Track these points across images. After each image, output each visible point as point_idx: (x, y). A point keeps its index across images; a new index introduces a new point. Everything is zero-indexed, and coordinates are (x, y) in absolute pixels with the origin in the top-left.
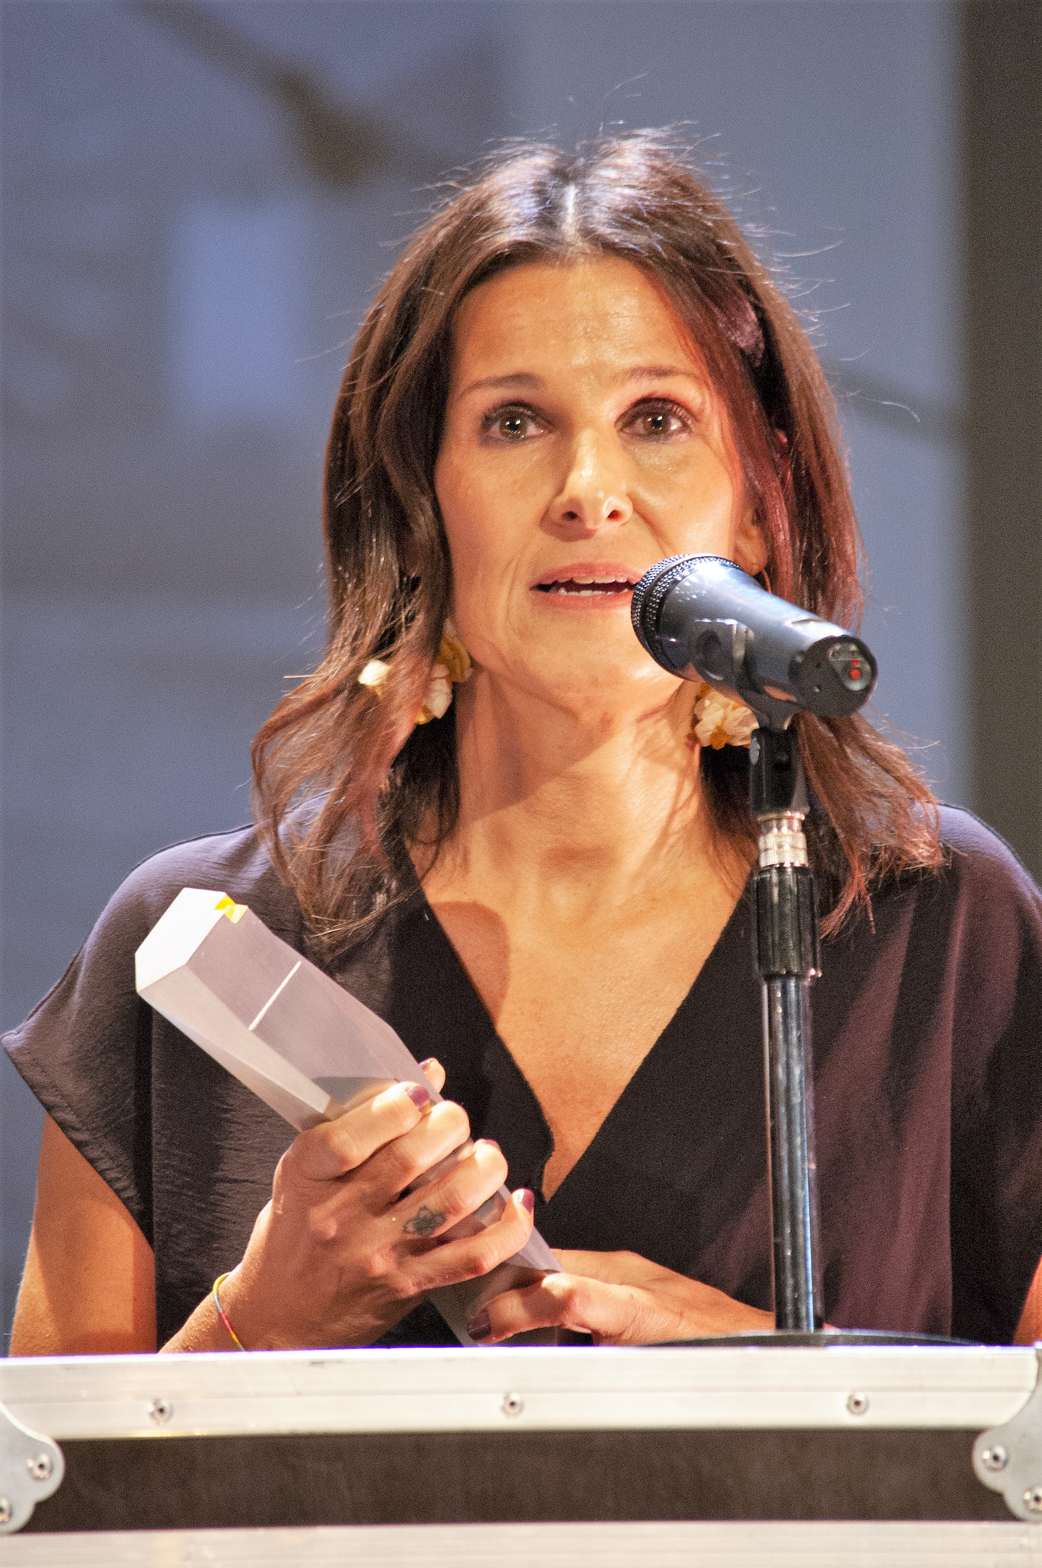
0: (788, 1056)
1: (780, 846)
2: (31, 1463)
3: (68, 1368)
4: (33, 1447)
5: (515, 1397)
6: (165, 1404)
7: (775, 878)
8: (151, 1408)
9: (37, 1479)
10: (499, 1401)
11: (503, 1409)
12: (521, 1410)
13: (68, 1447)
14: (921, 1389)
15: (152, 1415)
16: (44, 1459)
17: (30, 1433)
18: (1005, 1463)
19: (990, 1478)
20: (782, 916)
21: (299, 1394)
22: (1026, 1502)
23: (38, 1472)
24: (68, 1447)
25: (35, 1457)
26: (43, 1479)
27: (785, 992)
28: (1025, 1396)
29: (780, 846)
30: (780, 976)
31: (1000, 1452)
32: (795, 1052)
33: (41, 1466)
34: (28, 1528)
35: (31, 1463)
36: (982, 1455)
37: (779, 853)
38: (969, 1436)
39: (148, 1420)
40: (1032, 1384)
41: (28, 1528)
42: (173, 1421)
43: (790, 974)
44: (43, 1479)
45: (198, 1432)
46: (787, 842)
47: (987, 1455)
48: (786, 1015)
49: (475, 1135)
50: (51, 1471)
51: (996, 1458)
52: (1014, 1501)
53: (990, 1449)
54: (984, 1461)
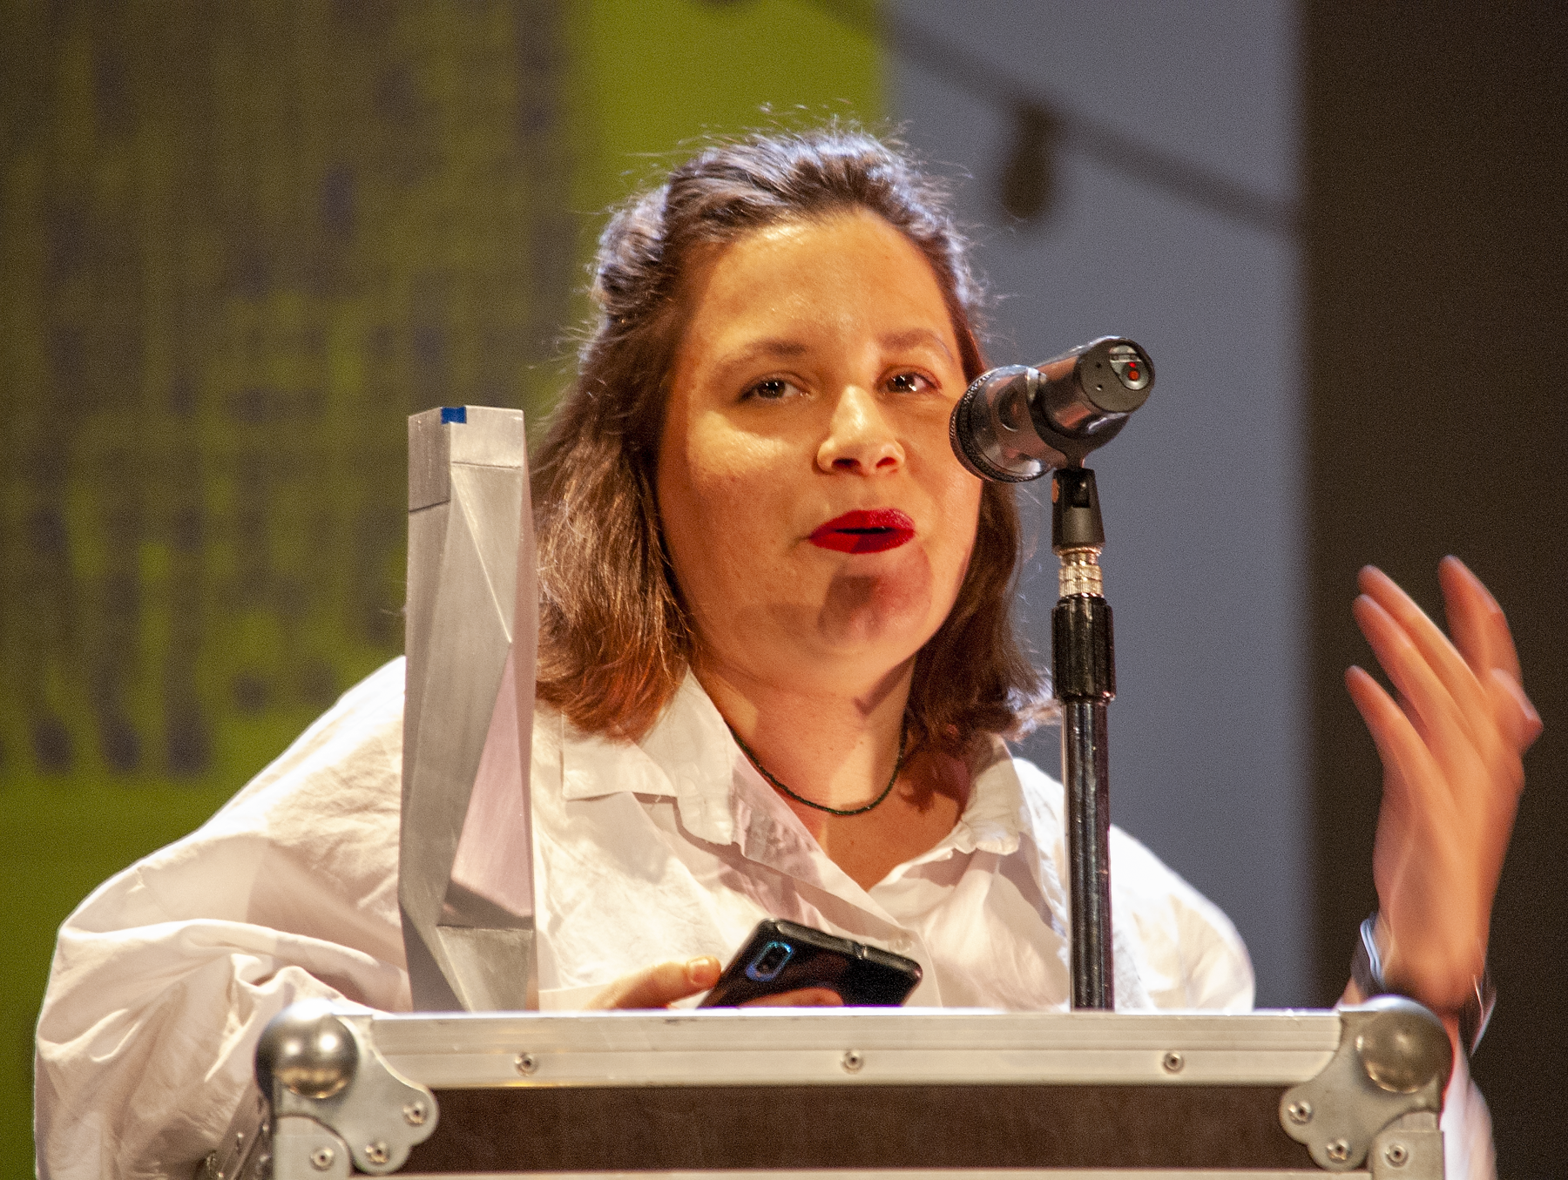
0: (1084, 770)
1: (1078, 578)
2: (407, 1110)
3: (441, 1023)
4: (408, 1095)
5: (855, 1054)
6: (530, 1057)
7: (1073, 609)
8: (518, 1061)
9: (413, 1124)
10: (840, 1057)
11: (845, 1065)
12: (1182, 1066)
13: (440, 1094)
14: (1233, 1048)
15: (519, 1067)
16: (419, 1106)
17: (406, 1082)
18: (1310, 1116)
19: (1295, 1131)
20: (1079, 642)
21: (654, 1049)
22: (1329, 1152)
23: (414, 1119)
24: (440, 1094)
25: (411, 1104)
26: (417, 1125)
27: (1081, 710)
28: (1329, 1055)
29: (1078, 578)
30: (1075, 696)
31: (1306, 1106)
32: (1090, 768)
33: (417, 1113)
34: (404, 1169)
35: (407, 1110)
36: (1289, 1109)
37: (1077, 585)
38: (1278, 1091)
39: (515, 1072)
40: (1335, 1044)
41: (404, 1169)
42: (539, 1073)
43: (1086, 696)
44: (417, 1125)
45: (562, 1084)
46: (1085, 574)
47: (1293, 1109)
48: (1082, 733)
49: (599, 247)
50: (426, 1117)
51: (1302, 1112)
52: (1318, 1152)
53: (1296, 1104)
54: (1291, 1114)
